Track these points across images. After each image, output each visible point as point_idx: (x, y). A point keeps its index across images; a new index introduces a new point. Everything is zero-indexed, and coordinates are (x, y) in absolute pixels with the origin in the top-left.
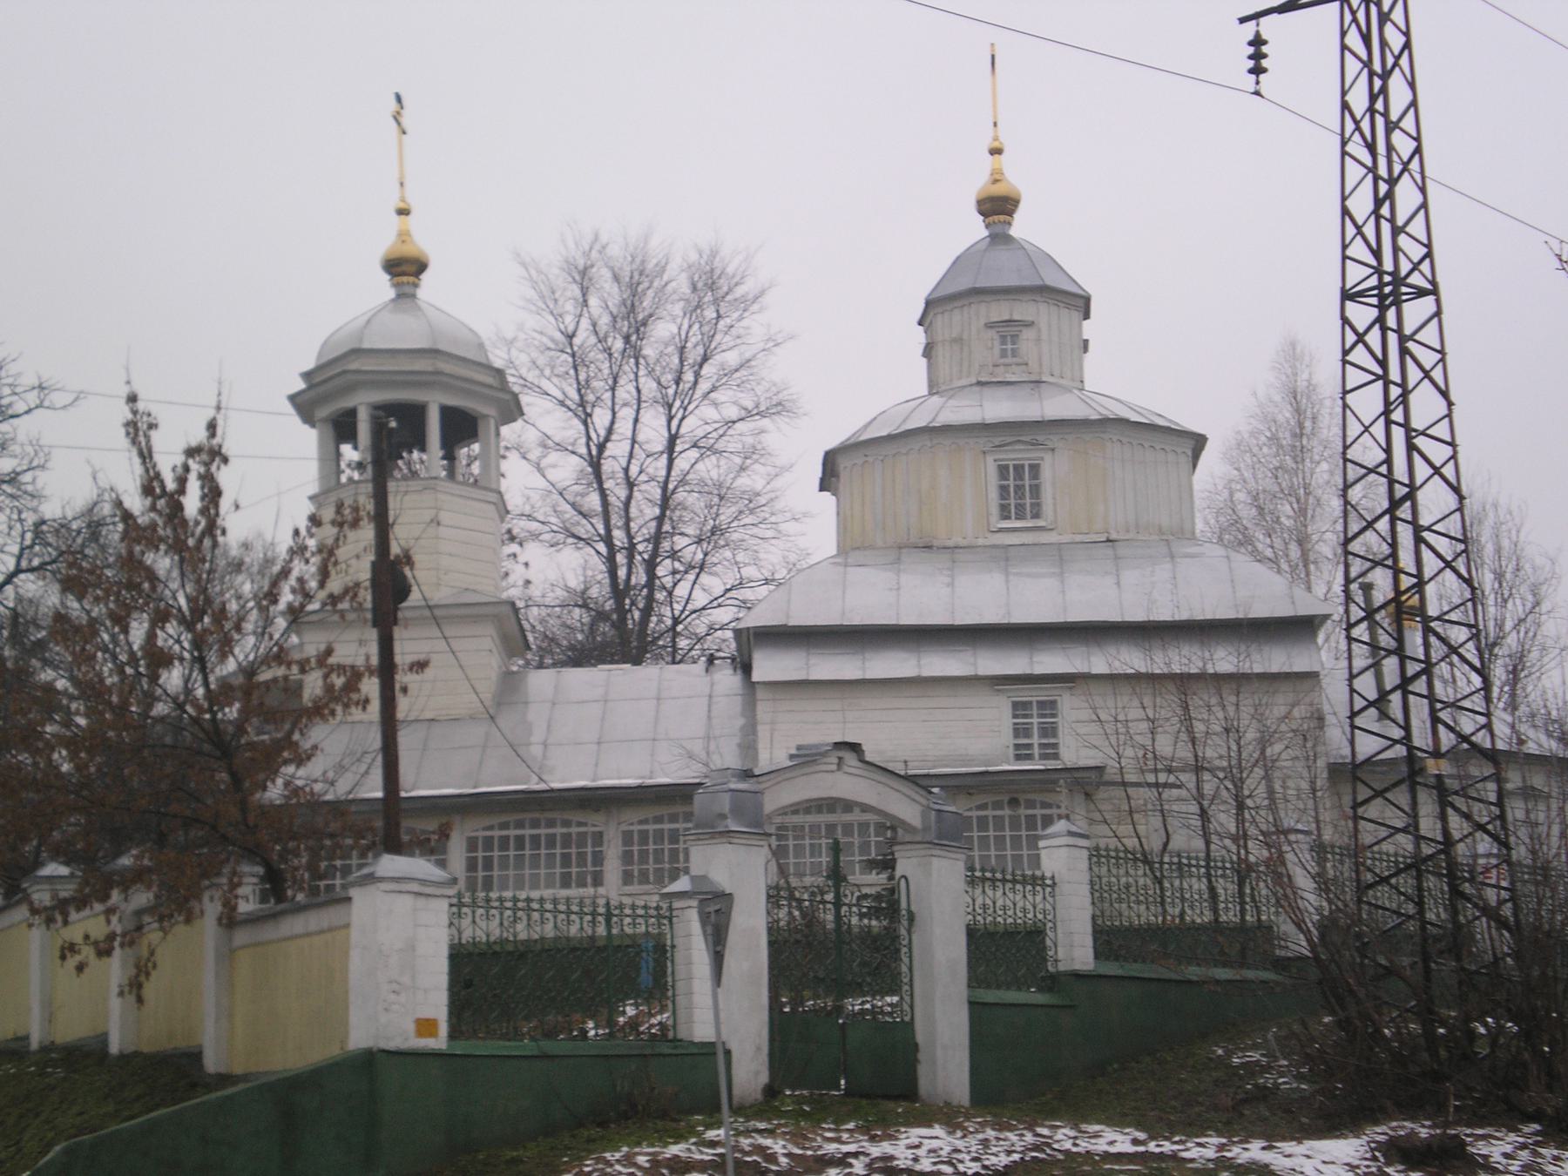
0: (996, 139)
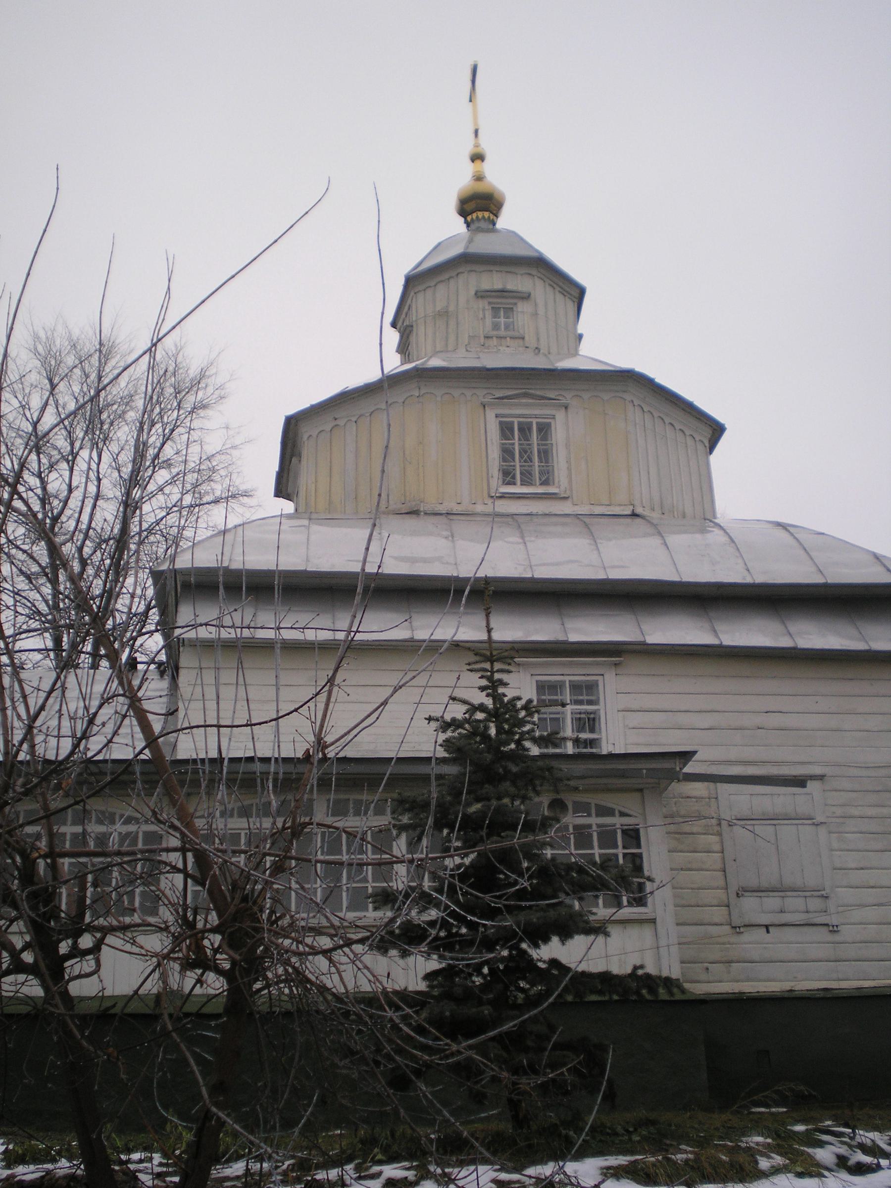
0: (477, 146)
